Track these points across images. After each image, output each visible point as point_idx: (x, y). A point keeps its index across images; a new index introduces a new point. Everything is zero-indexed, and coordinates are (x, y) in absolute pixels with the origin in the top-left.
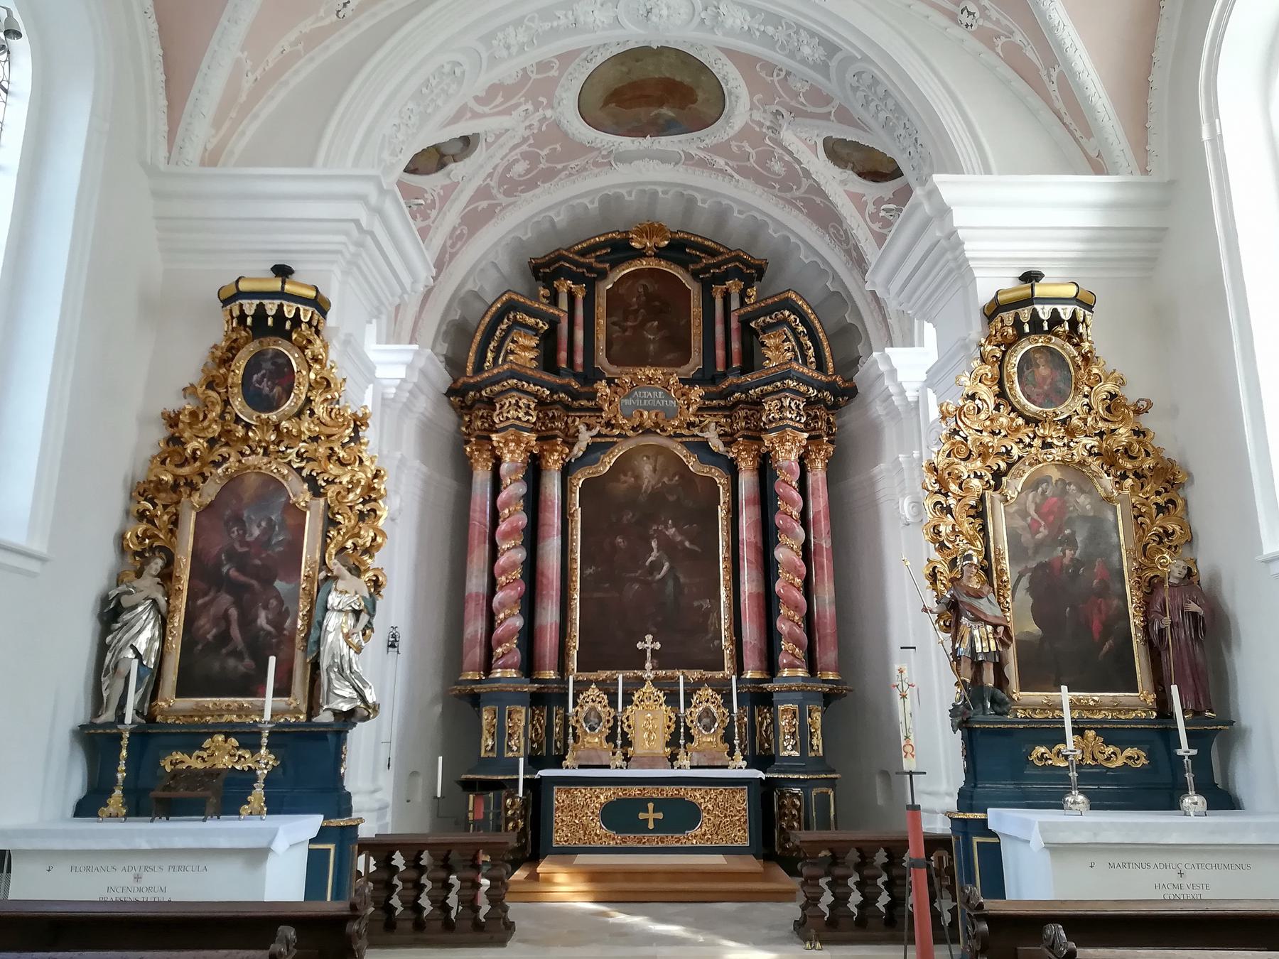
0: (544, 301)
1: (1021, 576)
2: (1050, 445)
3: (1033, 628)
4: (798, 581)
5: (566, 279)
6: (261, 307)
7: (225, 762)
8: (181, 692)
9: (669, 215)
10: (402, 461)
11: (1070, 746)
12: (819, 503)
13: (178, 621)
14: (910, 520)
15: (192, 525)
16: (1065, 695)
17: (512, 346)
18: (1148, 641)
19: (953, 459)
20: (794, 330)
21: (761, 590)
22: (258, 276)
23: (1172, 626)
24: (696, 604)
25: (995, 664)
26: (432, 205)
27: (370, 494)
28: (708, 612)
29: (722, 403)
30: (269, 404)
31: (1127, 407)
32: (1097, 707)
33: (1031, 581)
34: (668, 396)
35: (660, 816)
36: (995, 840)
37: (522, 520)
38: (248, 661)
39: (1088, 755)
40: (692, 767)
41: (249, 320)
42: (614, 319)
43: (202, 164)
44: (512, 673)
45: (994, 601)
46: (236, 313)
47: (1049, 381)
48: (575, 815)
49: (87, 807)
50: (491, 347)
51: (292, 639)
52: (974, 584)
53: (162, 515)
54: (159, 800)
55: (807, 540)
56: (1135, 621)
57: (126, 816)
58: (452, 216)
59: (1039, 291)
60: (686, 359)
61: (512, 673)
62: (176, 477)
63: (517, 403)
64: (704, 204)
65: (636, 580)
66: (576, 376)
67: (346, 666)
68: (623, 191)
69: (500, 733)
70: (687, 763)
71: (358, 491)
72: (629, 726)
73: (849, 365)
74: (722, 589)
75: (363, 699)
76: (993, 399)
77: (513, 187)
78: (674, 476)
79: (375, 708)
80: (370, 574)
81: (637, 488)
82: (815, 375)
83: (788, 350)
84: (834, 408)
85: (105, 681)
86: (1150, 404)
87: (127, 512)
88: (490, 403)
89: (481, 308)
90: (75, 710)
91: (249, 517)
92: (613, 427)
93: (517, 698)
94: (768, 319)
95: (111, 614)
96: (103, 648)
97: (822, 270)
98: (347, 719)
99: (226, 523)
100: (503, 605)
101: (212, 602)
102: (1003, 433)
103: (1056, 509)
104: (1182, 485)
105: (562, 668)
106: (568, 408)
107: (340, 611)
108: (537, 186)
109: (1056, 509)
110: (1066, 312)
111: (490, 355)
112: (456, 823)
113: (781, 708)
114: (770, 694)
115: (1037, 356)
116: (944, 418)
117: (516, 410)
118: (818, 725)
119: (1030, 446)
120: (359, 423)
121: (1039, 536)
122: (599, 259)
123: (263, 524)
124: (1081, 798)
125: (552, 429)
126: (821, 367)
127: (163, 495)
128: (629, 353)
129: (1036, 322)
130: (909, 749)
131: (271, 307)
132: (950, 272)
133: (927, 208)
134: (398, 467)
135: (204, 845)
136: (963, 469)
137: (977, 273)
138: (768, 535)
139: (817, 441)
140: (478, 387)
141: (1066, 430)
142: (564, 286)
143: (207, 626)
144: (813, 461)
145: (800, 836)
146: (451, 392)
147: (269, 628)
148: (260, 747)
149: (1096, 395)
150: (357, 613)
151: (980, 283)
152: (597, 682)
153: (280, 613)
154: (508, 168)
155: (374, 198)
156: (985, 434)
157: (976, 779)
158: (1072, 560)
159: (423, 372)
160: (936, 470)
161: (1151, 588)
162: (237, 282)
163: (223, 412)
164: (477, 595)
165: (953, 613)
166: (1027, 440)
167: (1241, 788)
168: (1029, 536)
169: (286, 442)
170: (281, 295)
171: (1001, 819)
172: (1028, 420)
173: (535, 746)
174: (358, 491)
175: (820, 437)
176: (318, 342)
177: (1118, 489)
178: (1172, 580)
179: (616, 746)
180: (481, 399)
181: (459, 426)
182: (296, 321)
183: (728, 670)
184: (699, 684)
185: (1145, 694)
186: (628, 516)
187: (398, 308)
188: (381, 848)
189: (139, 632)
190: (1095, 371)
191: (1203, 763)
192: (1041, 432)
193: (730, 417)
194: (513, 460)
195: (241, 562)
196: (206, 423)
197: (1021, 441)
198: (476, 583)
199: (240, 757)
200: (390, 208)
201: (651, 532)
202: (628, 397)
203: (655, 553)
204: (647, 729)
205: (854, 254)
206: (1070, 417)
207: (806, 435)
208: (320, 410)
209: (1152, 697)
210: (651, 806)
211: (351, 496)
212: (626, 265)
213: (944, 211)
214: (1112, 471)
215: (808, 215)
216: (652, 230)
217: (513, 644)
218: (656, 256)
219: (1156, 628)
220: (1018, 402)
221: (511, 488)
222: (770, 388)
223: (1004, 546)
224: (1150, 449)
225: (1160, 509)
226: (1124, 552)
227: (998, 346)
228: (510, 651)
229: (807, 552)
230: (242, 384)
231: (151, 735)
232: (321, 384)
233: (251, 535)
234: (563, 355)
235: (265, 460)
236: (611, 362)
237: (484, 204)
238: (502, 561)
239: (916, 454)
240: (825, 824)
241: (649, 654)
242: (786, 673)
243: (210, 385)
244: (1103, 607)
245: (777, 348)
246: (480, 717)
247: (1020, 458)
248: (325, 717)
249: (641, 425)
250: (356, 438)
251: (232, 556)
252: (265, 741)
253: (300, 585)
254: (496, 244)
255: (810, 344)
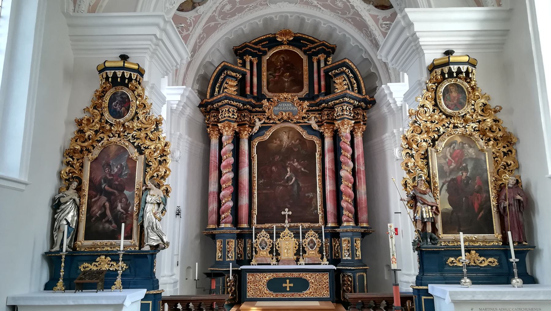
0: (240, 65)
1: (444, 184)
2: (457, 127)
3: (449, 207)
4: (350, 185)
5: (249, 55)
6: (115, 74)
7: (105, 267)
8: (87, 238)
9: (293, 26)
10: (180, 136)
11: (463, 257)
12: (359, 151)
13: (84, 208)
14: (399, 158)
15: (89, 168)
16: (462, 236)
17: (226, 85)
18: (499, 211)
19: (414, 134)
20: (348, 76)
21: (335, 189)
22: (114, 60)
23: (509, 205)
24: (307, 195)
25: (432, 223)
26: (190, 25)
27: (163, 154)
28: (312, 198)
29: (317, 108)
30: (120, 115)
31: (491, 110)
32: (477, 241)
33: (448, 187)
34: (294, 106)
35: (292, 285)
36: (432, 298)
37: (232, 160)
38: (114, 225)
39: (472, 261)
40: (305, 264)
41: (110, 79)
42: (270, 72)
43: (89, 12)
44: (229, 225)
45: (432, 195)
46: (105, 76)
47: (456, 99)
48: (256, 285)
49: (49, 286)
50: (217, 86)
51: (132, 215)
52: (423, 188)
53: (76, 163)
54: (78, 284)
55: (354, 167)
56: (493, 203)
57: (66, 289)
58: (199, 30)
59: (452, 59)
60: (301, 89)
61: (229, 225)
62: (82, 147)
63: (229, 110)
64: (308, 21)
65: (281, 185)
66: (254, 98)
67: (155, 226)
68: (273, 16)
69: (224, 251)
70: (304, 263)
71: (158, 152)
72: (279, 247)
73: (372, 90)
74: (318, 188)
75: (162, 240)
76: (432, 107)
77: (225, 16)
78: (297, 140)
79: (168, 244)
80: (164, 187)
81: (281, 146)
82: (357, 95)
83: (345, 85)
84: (366, 109)
85: (55, 234)
86: (501, 108)
87: (62, 162)
88: (217, 110)
89: (213, 68)
90: (43, 246)
91: (112, 164)
92: (270, 119)
93: (231, 236)
94: (336, 71)
95: (57, 206)
96: (54, 220)
97: (360, 49)
98: (156, 248)
99: (103, 166)
100: (224, 197)
101: (98, 200)
102: (436, 122)
103: (459, 155)
104: (515, 144)
105: (250, 222)
106: (251, 112)
107: (151, 203)
108: (235, 15)
109: (459, 155)
110: (464, 68)
111: (217, 90)
112: (204, 290)
113: (343, 239)
114: (339, 233)
115: (451, 88)
116: (410, 116)
117: (228, 113)
118: (359, 246)
119: (448, 127)
120: (158, 123)
121: (452, 167)
122: (263, 46)
123: (119, 166)
124: (468, 280)
125: (244, 121)
126: (360, 92)
127: (77, 155)
128: (277, 87)
129: (450, 73)
130: (394, 260)
131: (119, 73)
132: (413, 51)
133: (403, 23)
134: (178, 139)
135: (96, 303)
136: (419, 138)
137: (425, 52)
138: (337, 165)
139: (358, 124)
140: (212, 103)
141: (464, 120)
142: (248, 58)
143: (97, 210)
144: (356, 133)
145: (349, 296)
146: (200, 106)
147: (122, 210)
148: (119, 261)
149: (477, 104)
150: (159, 204)
151: (426, 56)
152: (265, 229)
153: (126, 205)
154: (223, 8)
155: (162, 24)
156: (428, 123)
157: (423, 272)
158: (466, 177)
159: (188, 98)
160: (407, 138)
161: (500, 188)
162: (105, 63)
163: (101, 119)
164: (214, 192)
165: (414, 201)
166: (447, 125)
167: (539, 275)
168: (447, 167)
169: (127, 131)
170: (123, 68)
171: (435, 289)
172: (447, 116)
173: (239, 256)
174: (158, 152)
175: (360, 122)
176: (140, 88)
177: (486, 146)
178: (509, 185)
179: (273, 256)
180: (213, 109)
181: (205, 120)
182: (130, 79)
183: (321, 223)
184: (308, 229)
185: (497, 235)
186: (277, 158)
187: (177, 70)
188: (172, 302)
189: (68, 213)
190: (477, 94)
191: (521, 264)
192: (452, 121)
193: (321, 114)
194: (227, 135)
195: (110, 183)
196: (94, 124)
197: (444, 125)
198: (213, 187)
199: (112, 265)
200: (169, 28)
201: (287, 164)
202: (276, 106)
203: (289, 174)
204: (286, 248)
205: (374, 42)
206: (466, 114)
207: (353, 122)
208: (141, 117)
209: (501, 236)
210: (288, 281)
211: (156, 154)
212: (275, 48)
213: (410, 25)
214: (484, 138)
215: (354, 25)
216: (285, 33)
217: (229, 213)
218: (288, 44)
219: (502, 206)
220: (443, 108)
221: (227, 146)
222: (337, 101)
223: (436, 171)
224: (501, 128)
225: (505, 154)
226: (488, 173)
227: (434, 83)
228: (227, 216)
229: (354, 172)
230: (108, 107)
231: (75, 257)
232: (142, 106)
233: (114, 171)
234: (248, 89)
235: (119, 139)
236: (269, 91)
237: (213, 24)
238: (223, 178)
239: (401, 129)
240: (362, 291)
241: (287, 217)
242: (345, 224)
243: (95, 108)
244: (480, 198)
245: (341, 84)
246: (216, 244)
247: (444, 133)
248: (146, 248)
249: (282, 118)
250: (157, 129)
251: (106, 180)
252: (121, 259)
253: (134, 192)
254: (219, 41)
255: (355, 82)
